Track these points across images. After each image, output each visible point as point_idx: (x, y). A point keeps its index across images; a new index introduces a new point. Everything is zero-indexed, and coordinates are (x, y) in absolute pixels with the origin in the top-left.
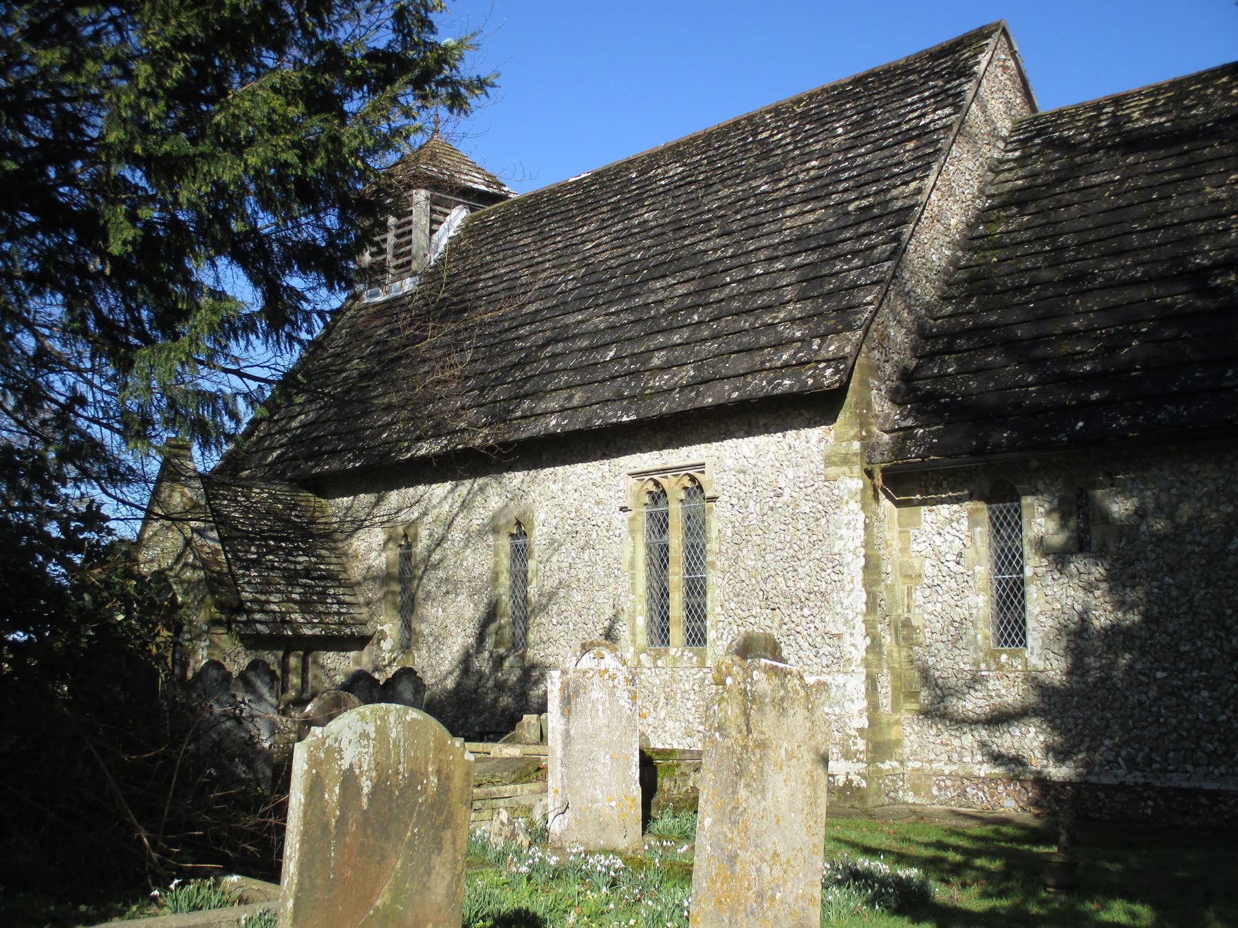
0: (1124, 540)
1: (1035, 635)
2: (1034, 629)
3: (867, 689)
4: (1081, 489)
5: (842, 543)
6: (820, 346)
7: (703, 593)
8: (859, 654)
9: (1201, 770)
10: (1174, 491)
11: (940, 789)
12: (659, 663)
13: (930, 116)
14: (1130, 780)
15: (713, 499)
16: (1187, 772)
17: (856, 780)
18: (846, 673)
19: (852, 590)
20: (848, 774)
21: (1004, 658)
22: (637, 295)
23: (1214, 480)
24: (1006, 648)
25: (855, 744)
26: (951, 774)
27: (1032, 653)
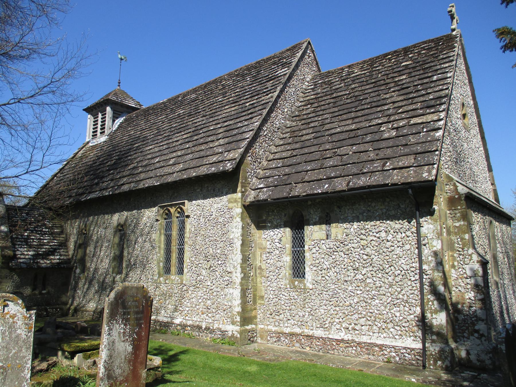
0: (345, 234)
1: (309, 274)
2: (308, 272)
3: (241, 295)
4: (328, 213)
5: (233, 234)
6: (227, 155)
7: (183, 254)
8: (238, 281)
9: (376, 335)
10: (365, 214)
11: (271, 337)
12: (167, 282)
13: (280, 72)
14: (346, 338)
15: (188, 217)
16: (370, 335)
17: (236, 333)
18: (233, 288)
19: (236, 254)
20: (233, 331)
21: (296, 283)
22: (171, 139)
23: (381, 209)
24: (297, 279)
25: (236, 318)
26: (275, 331)
27: (307, 281)
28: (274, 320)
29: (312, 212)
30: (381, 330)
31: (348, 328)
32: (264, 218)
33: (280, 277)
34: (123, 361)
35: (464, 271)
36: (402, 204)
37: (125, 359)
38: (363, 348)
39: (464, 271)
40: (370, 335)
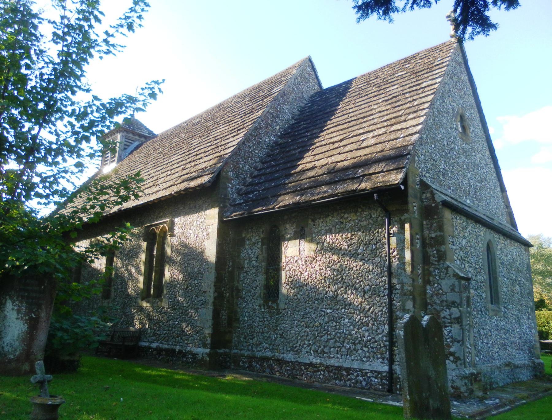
4: (302, 228)
10: (338, 226)
14: (314, 361)
16: (338, 358)
26: (247, 356)
28: (248, 344)
29: (288, 226)
30: (349, 352)
31: (317, 351)
32: (244, 235)
33: (255, 297)
34: (15, 338)
35: (440, 287)
36: (374, 214)
37: (18, 337)
38: (331, 372)
39: (440, 287)
40: (338, 358)
